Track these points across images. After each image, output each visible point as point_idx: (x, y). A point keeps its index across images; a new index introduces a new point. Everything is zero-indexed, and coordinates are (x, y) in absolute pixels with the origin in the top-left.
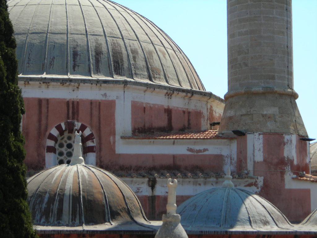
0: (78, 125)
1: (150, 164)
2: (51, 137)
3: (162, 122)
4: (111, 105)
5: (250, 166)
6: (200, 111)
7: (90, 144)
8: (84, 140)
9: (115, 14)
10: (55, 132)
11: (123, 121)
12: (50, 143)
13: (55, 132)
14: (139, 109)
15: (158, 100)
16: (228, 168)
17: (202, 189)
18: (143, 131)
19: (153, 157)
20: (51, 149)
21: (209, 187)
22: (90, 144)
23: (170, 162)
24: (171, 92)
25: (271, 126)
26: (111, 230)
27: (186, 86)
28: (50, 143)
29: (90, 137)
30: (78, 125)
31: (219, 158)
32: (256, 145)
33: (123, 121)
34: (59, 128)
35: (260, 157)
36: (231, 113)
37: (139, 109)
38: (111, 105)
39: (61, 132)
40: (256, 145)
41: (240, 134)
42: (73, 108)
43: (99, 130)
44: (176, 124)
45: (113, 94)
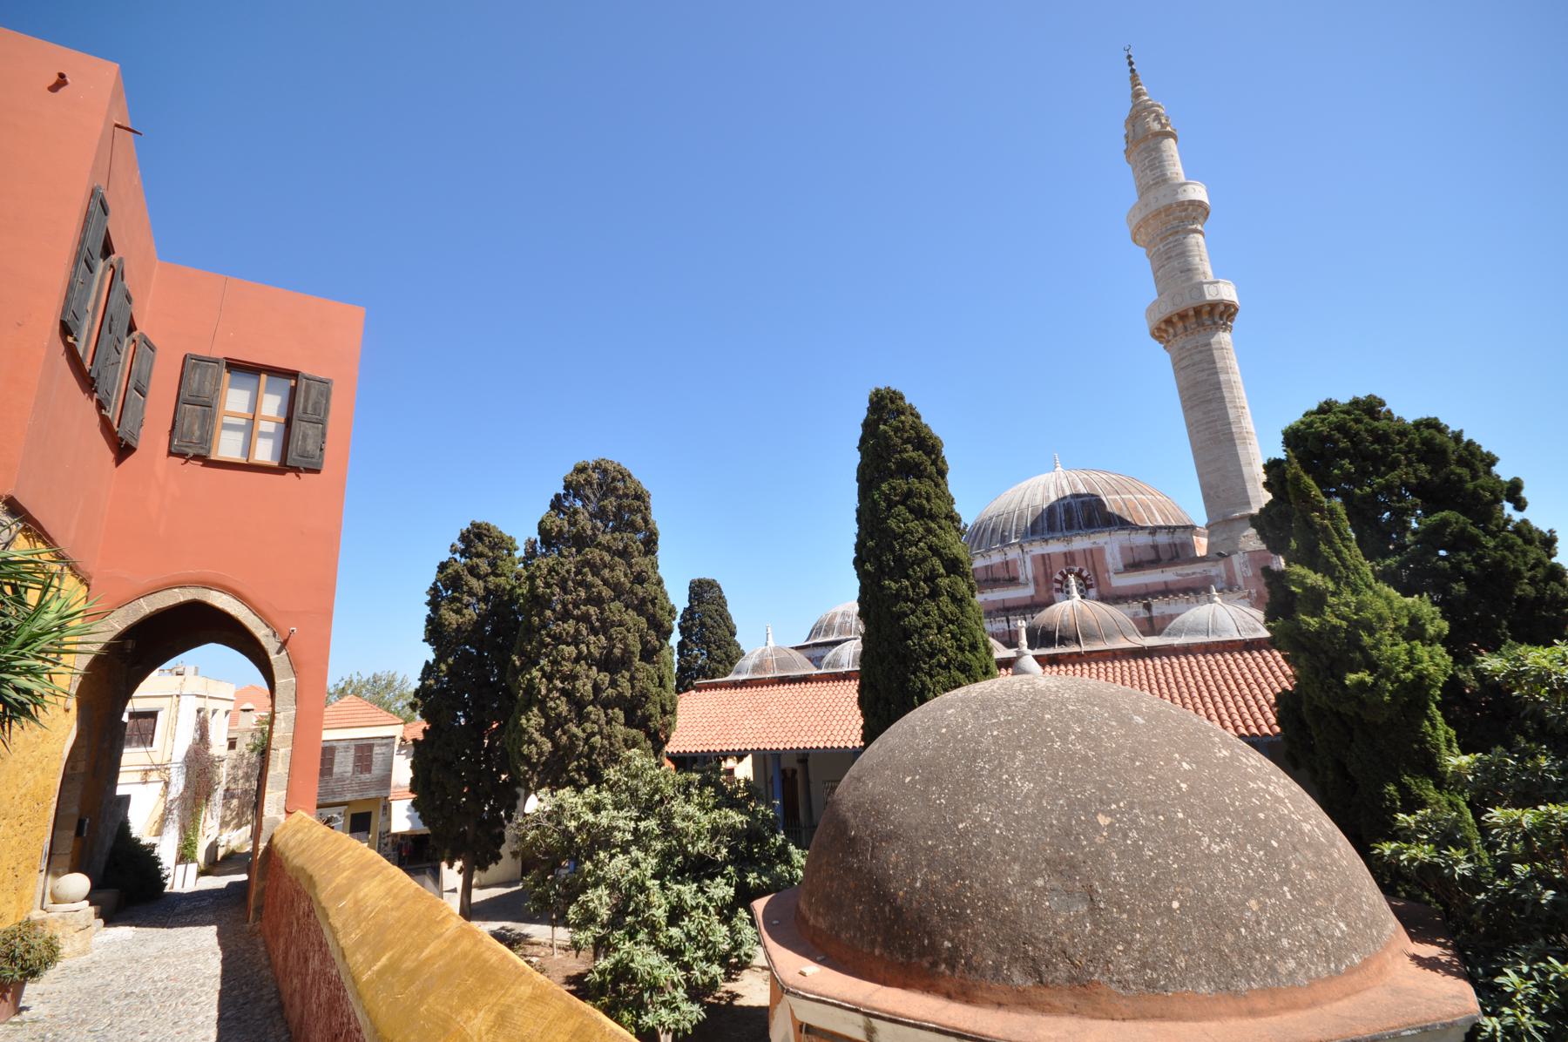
3: (1151, 555)
10: (1059, 577)
13: (1059, 577)
18: (1134, 566)
38: (1101, 550)
44: (1164, 557)
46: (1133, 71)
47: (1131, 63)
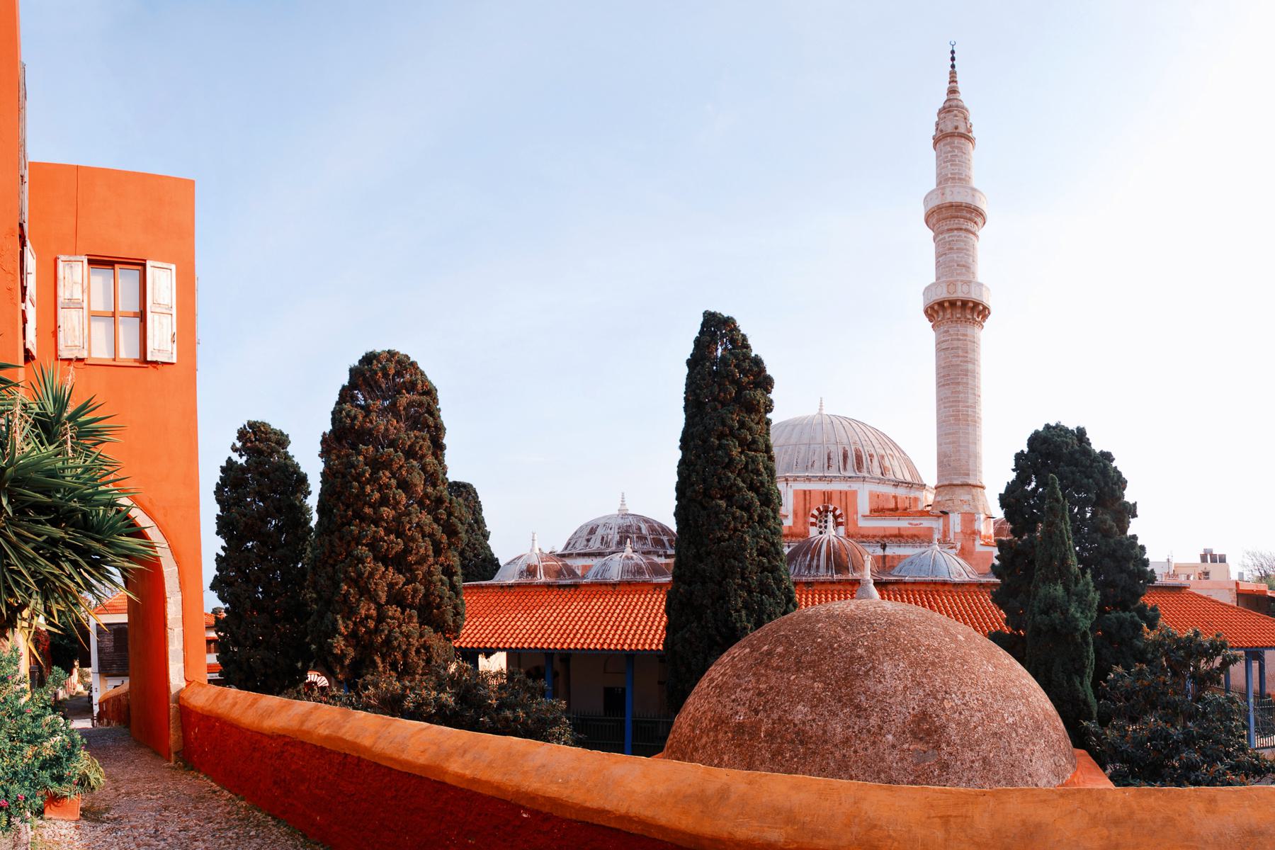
0: (831, 508)
1: (882, 533)
2: (813, 516)
4: (855, 493)
5: (952, 536)
6: (1024, 823)
7: (840, 520)
8: (836, 517)
9: (858, 430)
10: (816, 513)
11: (864, 505)
12: (813, 520)
13: (816, 513)
14: (875, 497)
15: (889, 490)
16: (936, 536)
17: (918, 551)
19: (875, 528)
20: (813, 524)
21: (923, 549)
22: (840, 520)
23: (896, 532)
24: (897, 484)
25: (966, 508)
26: (474, 788)
27: (909, 479)
28: (813, 520)
29: (840, 515)
30: (831, 508)
31: (930, 529)
32: (956, 521)
33: (864, 505)
34: (818, 509)
35: (958, 529)
36: (939, 498)
37: (875, 497)
38: (855, 493)
39: (820, 513)
40: (956, 521)
41: (945, 513)
42: (828, 496)
43: (846, 510)
45: (855, 486)
46: (953, 66)
47: (953, 59)
